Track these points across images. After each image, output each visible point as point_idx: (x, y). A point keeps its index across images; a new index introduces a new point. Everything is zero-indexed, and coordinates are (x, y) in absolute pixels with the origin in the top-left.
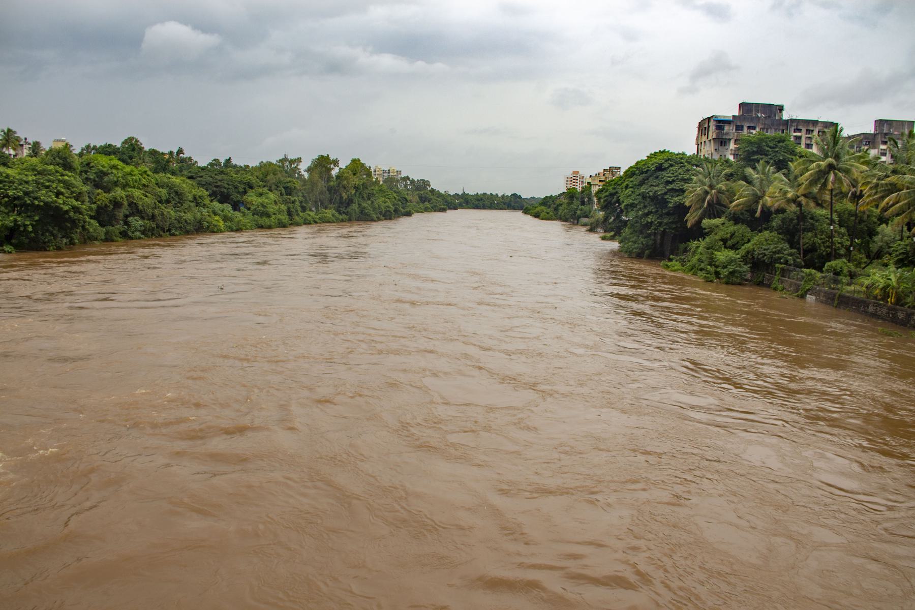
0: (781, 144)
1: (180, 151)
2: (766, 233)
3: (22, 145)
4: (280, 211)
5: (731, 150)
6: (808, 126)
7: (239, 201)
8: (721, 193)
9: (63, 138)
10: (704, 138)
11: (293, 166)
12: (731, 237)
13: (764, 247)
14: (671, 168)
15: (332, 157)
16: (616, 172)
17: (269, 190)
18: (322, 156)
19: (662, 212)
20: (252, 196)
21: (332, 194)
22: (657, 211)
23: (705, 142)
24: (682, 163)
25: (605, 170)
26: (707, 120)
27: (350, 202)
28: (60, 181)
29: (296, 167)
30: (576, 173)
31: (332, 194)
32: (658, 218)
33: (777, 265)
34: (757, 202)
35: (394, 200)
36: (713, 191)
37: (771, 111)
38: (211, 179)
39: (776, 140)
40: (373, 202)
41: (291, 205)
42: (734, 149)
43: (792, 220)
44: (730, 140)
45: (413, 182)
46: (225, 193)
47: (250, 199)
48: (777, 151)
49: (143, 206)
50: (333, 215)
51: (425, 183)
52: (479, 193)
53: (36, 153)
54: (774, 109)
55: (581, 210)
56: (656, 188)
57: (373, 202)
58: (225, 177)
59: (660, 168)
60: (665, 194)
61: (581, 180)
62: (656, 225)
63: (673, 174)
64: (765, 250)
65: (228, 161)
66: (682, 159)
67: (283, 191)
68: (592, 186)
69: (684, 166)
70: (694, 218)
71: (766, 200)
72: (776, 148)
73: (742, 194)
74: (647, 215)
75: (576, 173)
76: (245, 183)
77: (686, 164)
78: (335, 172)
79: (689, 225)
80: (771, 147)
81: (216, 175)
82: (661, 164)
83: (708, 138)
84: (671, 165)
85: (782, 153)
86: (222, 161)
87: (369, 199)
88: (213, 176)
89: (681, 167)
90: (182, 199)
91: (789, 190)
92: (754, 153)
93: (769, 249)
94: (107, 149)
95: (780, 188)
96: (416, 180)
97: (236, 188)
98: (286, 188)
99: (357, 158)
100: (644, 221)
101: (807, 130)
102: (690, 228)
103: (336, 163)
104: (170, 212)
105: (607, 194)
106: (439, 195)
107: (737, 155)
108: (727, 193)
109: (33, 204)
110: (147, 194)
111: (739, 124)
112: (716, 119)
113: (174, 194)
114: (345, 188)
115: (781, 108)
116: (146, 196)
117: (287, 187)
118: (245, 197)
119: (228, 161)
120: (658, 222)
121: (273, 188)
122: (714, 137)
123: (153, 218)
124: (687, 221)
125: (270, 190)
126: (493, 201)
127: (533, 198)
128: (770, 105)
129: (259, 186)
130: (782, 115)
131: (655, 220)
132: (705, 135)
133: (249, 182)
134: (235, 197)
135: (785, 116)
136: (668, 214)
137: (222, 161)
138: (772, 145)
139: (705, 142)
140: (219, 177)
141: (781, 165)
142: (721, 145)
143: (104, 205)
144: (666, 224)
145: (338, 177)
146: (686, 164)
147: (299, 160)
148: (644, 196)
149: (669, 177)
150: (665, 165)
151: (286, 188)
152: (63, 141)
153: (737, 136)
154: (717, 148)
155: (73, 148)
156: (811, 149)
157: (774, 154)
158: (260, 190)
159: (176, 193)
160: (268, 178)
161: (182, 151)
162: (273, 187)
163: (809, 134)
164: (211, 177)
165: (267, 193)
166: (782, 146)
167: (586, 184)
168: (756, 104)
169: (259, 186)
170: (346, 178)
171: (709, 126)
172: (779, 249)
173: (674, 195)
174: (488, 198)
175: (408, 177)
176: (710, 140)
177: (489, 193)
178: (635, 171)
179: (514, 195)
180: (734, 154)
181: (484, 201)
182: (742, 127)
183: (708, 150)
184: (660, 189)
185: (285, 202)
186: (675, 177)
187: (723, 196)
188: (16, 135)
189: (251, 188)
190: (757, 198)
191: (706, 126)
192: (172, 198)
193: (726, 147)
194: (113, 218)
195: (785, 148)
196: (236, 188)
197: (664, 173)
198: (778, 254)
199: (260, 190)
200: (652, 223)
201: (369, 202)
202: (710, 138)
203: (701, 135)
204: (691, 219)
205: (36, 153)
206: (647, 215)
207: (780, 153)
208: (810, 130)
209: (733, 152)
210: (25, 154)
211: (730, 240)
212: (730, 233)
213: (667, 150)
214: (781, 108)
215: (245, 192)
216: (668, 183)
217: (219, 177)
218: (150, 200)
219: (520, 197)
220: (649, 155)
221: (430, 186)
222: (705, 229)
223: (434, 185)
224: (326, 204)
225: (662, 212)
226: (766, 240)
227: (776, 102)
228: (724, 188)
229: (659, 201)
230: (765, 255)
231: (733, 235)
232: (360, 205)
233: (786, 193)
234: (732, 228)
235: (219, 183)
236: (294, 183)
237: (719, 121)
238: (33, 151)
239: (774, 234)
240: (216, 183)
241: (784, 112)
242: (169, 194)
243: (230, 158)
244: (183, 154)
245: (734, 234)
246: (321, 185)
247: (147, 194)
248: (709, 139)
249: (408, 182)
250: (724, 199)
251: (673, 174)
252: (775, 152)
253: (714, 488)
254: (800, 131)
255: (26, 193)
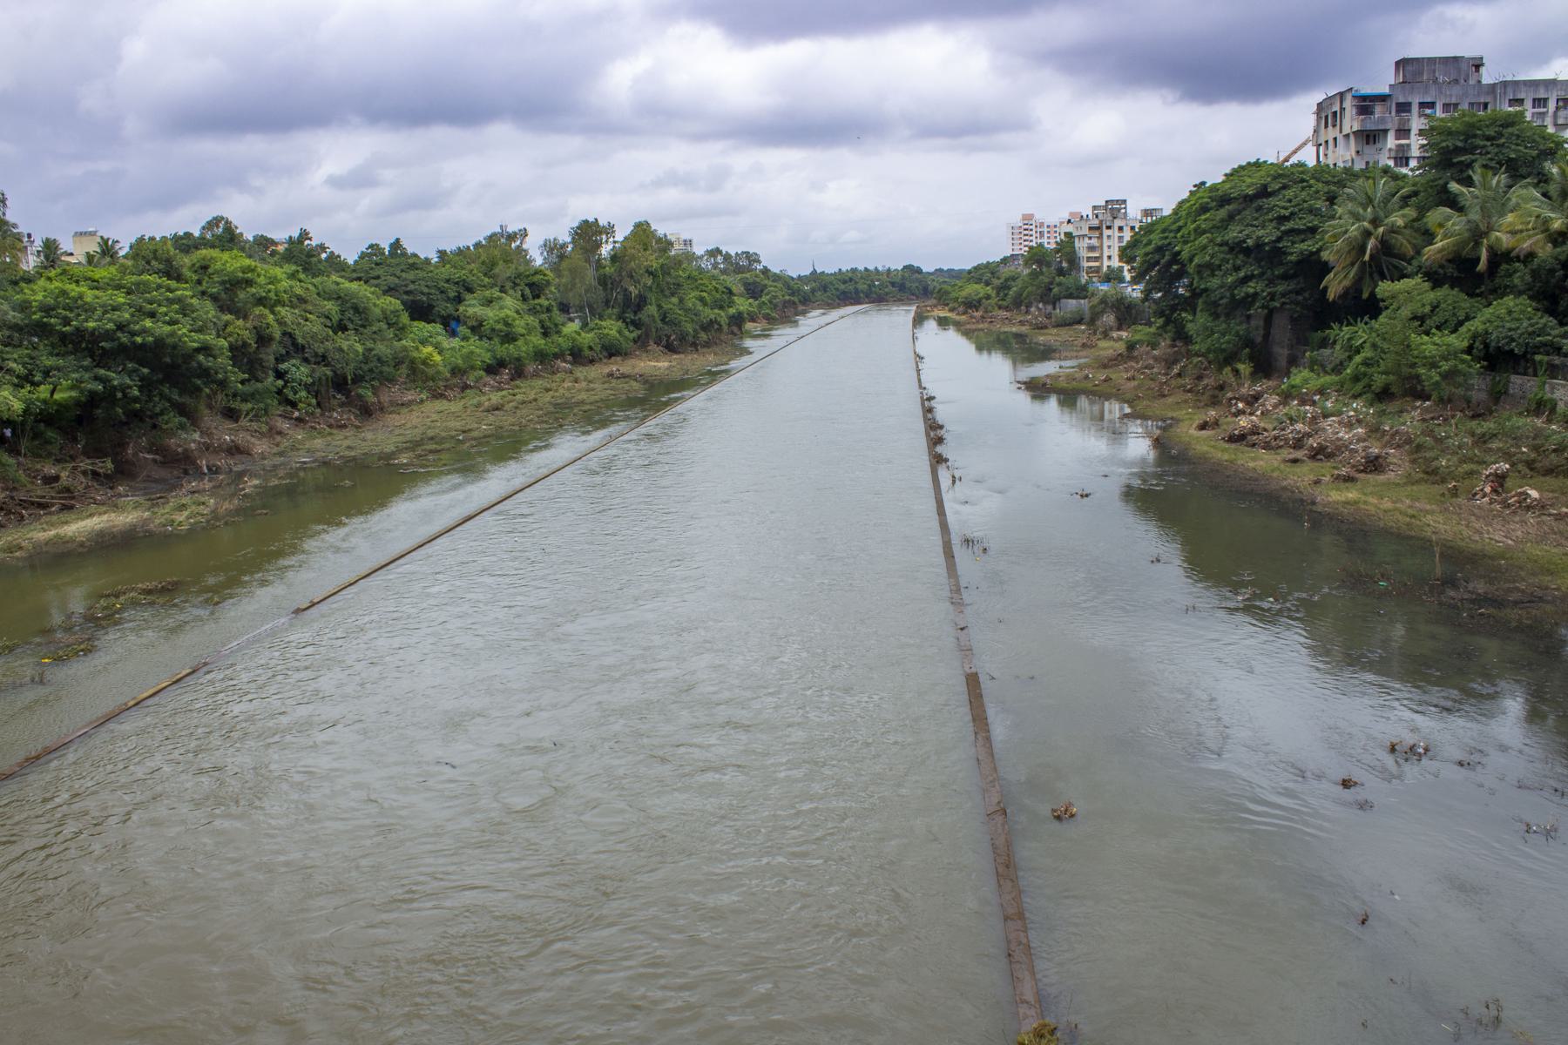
0: (1510, 130)
1: (304, 235)
2: (1509, 301)
3: (26, 247)
4: (530, 330)
5: (1390, 150)
6: (1535, 91)
7: (449, 316)
8: (1394, 232)
9: (91, 229)
10: (1332, 133)
11: (513, 245)
12: (1432, 311)
13: (1508, 325)
14: (1283, 192)
15: (602, 222)
16: (1119, 210)
17: (501, 291)
18: (586, 222)
19: (1273, 274)
20: (474, 306)
21: (609, 291)
22: (1262, 274)
23: (1335, 139)
24: (1303, 181)
25: (1095, 208)
26: (1338, 98)
27: (642, 302)
28: (171, 301)
29: (518, 247)
30: (1029, 217)
31: (609, 291)
32: (1267, 285)
33: (1538, 358)
34: (1477, 244)
35: (714, 293)
36: (1381, 230)
37: (1459, 70)
38: (396, 280)
39: (1498, 123)
40: (681, 300)
41: (544, 316)
42: (1394, 147)
43: (1552, 271)
44: (1386, 131)
45: (727, 257)
46: (423, 302)
47: (471, 311)
48: (1503, 145)
49: (304, 338)
50: (620, 332)
51: (752, 258)
52: (844, 270)
53: (53, 261)
54: (1464, 66)
55: (1059, 284)
56: (1261, 233)
57: (681, 300)
58: (421, 274)
59: (1264, 192)
60: (1279, 239)
61: (1039, 230)
62: (1265, 298)
63: (1290, 201)
64: (1510, 330)
65: (396, 245)
66: (1302, 173)
67: (527, 291)
68: (1076, 240)
69: (1310, 186)
70: (1340, 282)
71: (1497, 238)
72: (1499, 138)
73: (1448, 229)
74: (1245, 280)
75: (1028, 218)
76: (457, 283)
77: (1312, 182)
78: (606, 250)
79: (1331, 296)
80: (1488, 138)
81: (402, 271)
82: (1265, 187)
83: (1341, 132)
84: (1285, 187)
85: (1513, 147)
86: (386, 246)
87: (673, 294)
88: (398, 273)
89: (1303, 189)
90: (367, 320)
91: (1553, 215)
92: (1458, 151)
93: (1518, 328)
94: (184, 241)
95: (1536, 214)
96: (733, 254)
97: (442, 292)
98: (531, 285)
99: (642, 219)
100: (1240, 293)
101: (1534, 100)
102: (1334, 301)
103: (310, 239)
104: (350, 343)
105: (1150, 248)
106: (777, 278)
107: (1401, 158)
108: (1407, 232)
109: (134, 343)
110: (309, 316)
111: (1401, 100)
112: (1357, 94)
113: (352, 312)
114: (631, 277)
115: (1478, 65)
116: (307, 320)
117: (534, 284)
118: (461, 309)
119: (396, 245)
120: (1269, 294)
121: (507, 288)
122: (1355, 129)
123: (323, 359)
124: (1326, 289)
125: (503, 290)
126: (873, 281)
127: (940, 270)
128: (1456, 59)
129: (484, 286)
130: (1481, 76)
131: (1263, 291)
132: (1334, 126)
133: (464, 280)
134: (444, 308)
135: (1488, 77)
136: (1285, 277)
137: (386, 246)
138: (1493, 133)
139: (1335, 139)
140: (411, 275)
141: (1517, 170)
142: (1368, 143)
143: (240, 343)
144: (1283, 295)
145: (614, 258)
146: (1312, 182)
147: (524, 233)
148: (1237, 248)
149: (1284, 208)
150: (1272, 185)
151: (531, 285)
152: (93, 234)
153: (1400, 124)
154: (1360, 149)
155: (121, 245)
156: (1409, 138)
157: (1496, 150)
158: (487, 293)
159: (356, 309)
160: (496, 270)
161: (307, 234)
162: (508, 285)
163: (1539, 107)
164: (395, 275)
165: (500, 298)
166: (1512, 134)
167: (1063, 236)
168: (1429, 58)
169: (484, 286)
170: (633, 258)
171: (1342, 109)
172: (1540, 326)
173: (1297, 239)
174: (862, 278)
175: (718, 249)
176: (1347, 136)
177: (861, 268)
178: (1208, 203)
179: (909, 268)
180: (1395, 158)
181: (856, 283)
182: (1409, 104)
183: (1343, 156)
184: (1268, 234)
185: (533, 311)
186: (1296, 206)
187: (1400, 237)
188: (1207, 185)
189: (470, 290)
190: (1477, 235)
191: (1336, 108)
192: (349, 319)
193: (1378, 145)
194: (257, 366)
195: (1518, 137)
196: (442, 292)
197: (1272, 201)
198: (1539, 336)
199: (487, 293)
200: (1256, 295)
201: (675, 300)
202: (1346, 130)
203: (1326, 126)
204: (1335, 285)
205: (53, 261)
206: (1245, 280)
207: (1508, 147)
208: (1539, 100)
209: (1393, 154)
210: (32, 264)
211: (1430, 317)
212: (1431, 304)
213: (1261, 161)
214: (1478, 65)
215: (459, 300)
216: (1282, 219)
217: (411, 275)
218: (315, 326)
219: (919, 271)
220: (1228, 171)
221: (759, 262)
222: (1383, 301)
223: (766, 261)
224: (599, 311)
225: (1273, 274)
226: (1510, 312)
227: (1467, 51)
228: (1400, 222)
229: (1268, 255)
230: (1513, 340)
231: (1434, 308)
232: (659, 307)
233: (1546, 221)
234: (1432, 296)
235: (411, 287)
236: (545, 275)
237: (1364, 98)
238: (47, 257)
239: (1524, 299)
240: (406, 286)
241: (1483, 70)
242: (342, 312)
243: (398, 240)
244: (310, 239)
245: (1437, 306)
246: (590, 275)
247: (309, 316)
248: (1345, 132)
249: (719, 259)
250: (1404, 243)
251: (1290, 201)
252: (1498, 146)
253: (48, 856)
254: (1521, 102)
255: (121, 327)
